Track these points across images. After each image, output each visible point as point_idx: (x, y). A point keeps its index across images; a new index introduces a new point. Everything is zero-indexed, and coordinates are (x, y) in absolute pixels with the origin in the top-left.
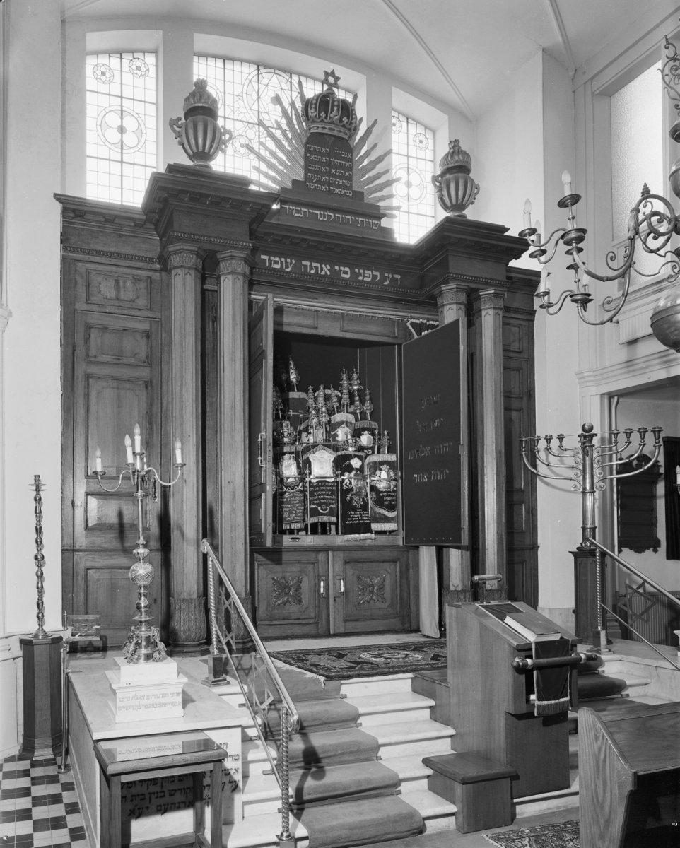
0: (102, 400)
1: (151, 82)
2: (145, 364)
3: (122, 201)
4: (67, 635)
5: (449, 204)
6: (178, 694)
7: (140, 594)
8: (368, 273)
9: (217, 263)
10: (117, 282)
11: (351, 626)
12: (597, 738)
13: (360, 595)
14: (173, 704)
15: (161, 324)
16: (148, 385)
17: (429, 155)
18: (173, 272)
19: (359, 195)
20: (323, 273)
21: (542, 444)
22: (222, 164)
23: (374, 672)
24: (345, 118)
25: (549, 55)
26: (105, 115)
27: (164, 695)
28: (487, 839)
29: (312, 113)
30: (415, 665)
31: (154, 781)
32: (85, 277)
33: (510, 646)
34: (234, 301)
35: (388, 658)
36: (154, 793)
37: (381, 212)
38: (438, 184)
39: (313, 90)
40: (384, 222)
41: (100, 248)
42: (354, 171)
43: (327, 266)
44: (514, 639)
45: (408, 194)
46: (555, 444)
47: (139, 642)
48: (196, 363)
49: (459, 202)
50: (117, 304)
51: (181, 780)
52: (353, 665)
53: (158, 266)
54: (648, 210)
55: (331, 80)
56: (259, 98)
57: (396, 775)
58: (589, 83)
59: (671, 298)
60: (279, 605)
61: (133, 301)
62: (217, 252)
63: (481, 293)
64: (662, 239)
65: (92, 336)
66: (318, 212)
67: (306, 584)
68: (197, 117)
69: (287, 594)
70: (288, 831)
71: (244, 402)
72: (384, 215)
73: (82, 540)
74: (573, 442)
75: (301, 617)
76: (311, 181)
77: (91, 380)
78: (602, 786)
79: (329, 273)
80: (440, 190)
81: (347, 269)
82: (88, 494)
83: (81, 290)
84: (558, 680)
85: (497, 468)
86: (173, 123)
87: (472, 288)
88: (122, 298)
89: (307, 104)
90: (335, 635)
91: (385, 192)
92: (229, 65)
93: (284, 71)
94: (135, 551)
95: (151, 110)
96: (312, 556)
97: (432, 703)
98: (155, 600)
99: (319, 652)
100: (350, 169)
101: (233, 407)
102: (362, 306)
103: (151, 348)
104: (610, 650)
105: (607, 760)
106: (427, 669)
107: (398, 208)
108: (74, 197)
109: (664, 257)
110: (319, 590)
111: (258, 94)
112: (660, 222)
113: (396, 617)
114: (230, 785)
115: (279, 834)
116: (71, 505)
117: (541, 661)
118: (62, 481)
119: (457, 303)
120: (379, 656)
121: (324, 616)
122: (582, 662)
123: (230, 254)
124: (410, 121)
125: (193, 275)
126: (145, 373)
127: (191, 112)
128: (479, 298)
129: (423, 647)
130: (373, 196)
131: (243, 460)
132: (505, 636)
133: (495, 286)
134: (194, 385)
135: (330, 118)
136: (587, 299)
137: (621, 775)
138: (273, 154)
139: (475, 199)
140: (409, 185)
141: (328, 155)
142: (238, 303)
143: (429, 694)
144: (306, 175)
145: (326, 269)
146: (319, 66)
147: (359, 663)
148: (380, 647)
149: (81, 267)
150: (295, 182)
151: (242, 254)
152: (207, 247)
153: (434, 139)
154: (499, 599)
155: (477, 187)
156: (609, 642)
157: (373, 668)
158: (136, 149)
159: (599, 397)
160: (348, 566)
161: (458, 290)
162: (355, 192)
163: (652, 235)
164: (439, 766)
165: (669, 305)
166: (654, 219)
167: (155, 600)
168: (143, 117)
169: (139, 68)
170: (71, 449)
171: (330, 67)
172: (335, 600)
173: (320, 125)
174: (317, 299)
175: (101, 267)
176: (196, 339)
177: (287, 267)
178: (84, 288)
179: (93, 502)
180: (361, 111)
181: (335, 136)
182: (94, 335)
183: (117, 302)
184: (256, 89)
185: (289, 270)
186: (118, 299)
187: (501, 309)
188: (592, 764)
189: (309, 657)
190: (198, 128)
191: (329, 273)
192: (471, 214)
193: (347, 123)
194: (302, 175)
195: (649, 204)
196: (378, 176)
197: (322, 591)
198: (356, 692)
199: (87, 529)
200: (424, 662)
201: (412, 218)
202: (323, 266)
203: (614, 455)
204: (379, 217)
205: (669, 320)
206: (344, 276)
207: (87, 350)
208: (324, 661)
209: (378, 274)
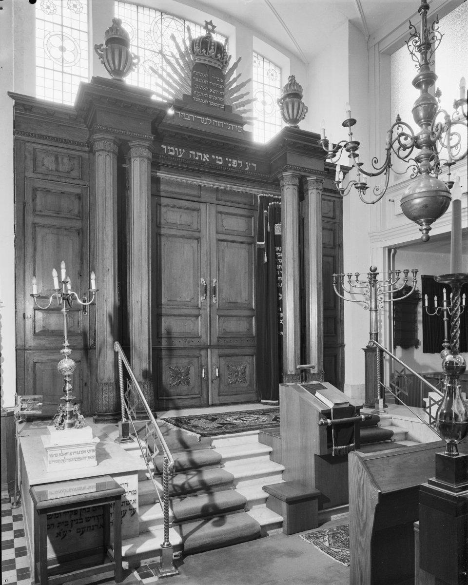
0: (46, 242)
1: (84, 17)
2: (78, 218)
3: (63, 101)
4: (17, 411)
5: (288, 119)
6: (93, 451)
7: (66, 381)
8: (235, 161)
9: (129, 149)
10: (57, 158)
11: (223, 399)
12: (359, 471)
13: (229, 378)
14: (89, 457)
15: (90, 190)
16: (80, 232)
17: (278, 85)
18: (97, 153)
19: (229, 108)
20: (204, 160)
21: (346, 279)
22: (131, 80)
23: (234, 430)
24: (204, 50)
25: (353, 24)
26: (50, 37)
27: (83, 452)
28: (302, 538)
29: (197, 49)
30: (262, 425)
31: (75, 512)
32: (32, 153)
33: (317, 411)
34: (140, 176)
35: (245, 420)
36: (75, 520)
37: (245, 121)
38: (281, 105)
39: (199, 33)
40: (246, 128)
41: (44, 133)
42: (226, 91)
43: (207, 155)
44: (321, 407)
45: (264, 109)
46: (354, 278)
47: (65, 415)
48: (114, 219)
49: (295, 117)
50: (57, 175)
51: (95, 510)
52: (221, 425)
53: (87, 149)
54: (400, 131)
55: (210, 27)
56: (162, 35)
57: (245, 498)
58: (377, 46)
59: (412, 188)
60: (174, 386)
61: (69, 172)
62: (130, 141)
63: (308, 179)
64: (408, 150)
65: (38, 197)
66: (201, 118)
67: (192, 371)
68: (114, 45)
69: (180, 378)
70: (168, 541)
71: (148, 246)
72: (246, 123)
73: (31, 341)
74: (364, 278)
75: (189, 394)
76: (196, 96)
77: (37, 228)
78: (361, 501)
79: (208, 160)
80: (282, 108)
81: (220, 158)
82: (35, 309)
83: (29, 163)
84: (347, 431)
85: (318, 295)
86: (97, 48)
87: (302, 175)
88: (60, 170)
89: (193, 43)
90: (213, 405)
91: (246, 107)
92: (141, 9)
93: (180, 18)
94: (62, 351)
95: (85, 37)
96: (197, 352)
97: (271, 449)
98: (86, 384)
99: (199, 418)
100: (223, 90)
101: (140, 250)
102: (231, 184)
103: (82, 206)
104: (385, 412)
105: (365, 485)
106: (269, 427)
107: (256, 119)
108: (26, 96)
109: (408, 162)
110: (201, 375)
111: (161, 32)
112: (406, 139)
113: (253, 393)
114: (130, 512)
115: (162, 544)
116: (22, 317)
117: (337, 420)
118: (16, 300)
119: (292, 185)
120: (239, 419)
121: (205, 393)
122: (363, 420)
123: (137, 143)
124: (265, 60)
125: (112, 156)
126: (78, 224)
127: (111, 41)
128: (307, 182)
129: (268, 412)
130: (238, 109)
131: (147, 287)
132: (315, 405)
133: (317, 174)
134: (112, 234)
135: (209, 54)
136: (365, 187)
137: (372, 494)
138: (169, 75)
139: (305, 116)
140: (264, 103)
141: (208, 79)
142: (144, 177)
143: (270, 444)
144: (192, 91)
145: (206, 157)
146: (204, 17)
147: (225, 424)
148: (241, 413)
149: (30, 147)
150: (184, 96)
151: (146, 144)
152: (123, 137)
153: (281, 73)
154: (319, 380)
155: (307, 109)
156: (385, 406)
157: (233, 427)
158: (73, 64)
159: (382, 249)
160: (221, 359)
161: (293, 176)
162: (226, 106)
163: (402, 148)
164: (273, 491)
165: (411, 193)
166: (402, 138)
167: (86, 384)
168: (78, 41)
169: (75, 6)
170: (23, 277)
171: (209, 18)
172: (212, 382)
173: (203, 58)
174: (200, 177)
175: (44, 147)
176: (113, 201)
177: (179, 154)
178: (32, 162)
179: (40, 315)
180: (231, 51)
181: (212, 66)
182: (39, 195)
183: (57, 172)
184: (160, 29)
185: (180, 156)
186: (57, 170)
187: (321, 190)
188: (356, 488)
189: (192, 421)
190: (115, 52)
191: (208, 160)
192: (303, 126)
193: (220, 58)
194: (190, 91)
195: (400, 128)
196: (241, 96)
197: (203, 376)
198: (223, 446)
199: (35, 333)
200: (268, 422)
201: (264, 127)
202: (204, 155)
203: (392, 286)
204: (242, 124)
205: (411, 203)
206: (218, 162)
207: (35, 205)
208: (202, 423)
209: (241, 162)
